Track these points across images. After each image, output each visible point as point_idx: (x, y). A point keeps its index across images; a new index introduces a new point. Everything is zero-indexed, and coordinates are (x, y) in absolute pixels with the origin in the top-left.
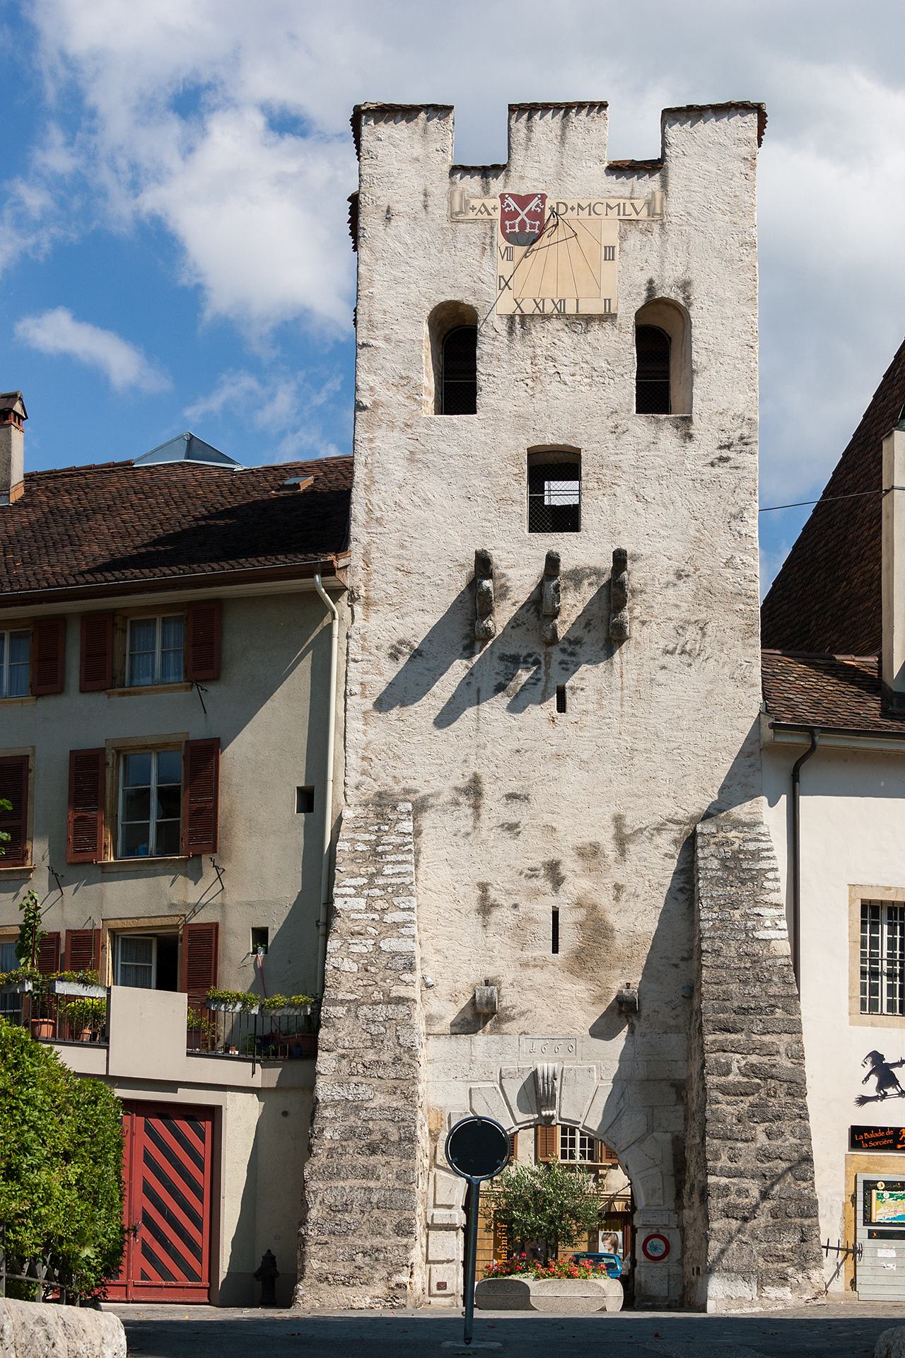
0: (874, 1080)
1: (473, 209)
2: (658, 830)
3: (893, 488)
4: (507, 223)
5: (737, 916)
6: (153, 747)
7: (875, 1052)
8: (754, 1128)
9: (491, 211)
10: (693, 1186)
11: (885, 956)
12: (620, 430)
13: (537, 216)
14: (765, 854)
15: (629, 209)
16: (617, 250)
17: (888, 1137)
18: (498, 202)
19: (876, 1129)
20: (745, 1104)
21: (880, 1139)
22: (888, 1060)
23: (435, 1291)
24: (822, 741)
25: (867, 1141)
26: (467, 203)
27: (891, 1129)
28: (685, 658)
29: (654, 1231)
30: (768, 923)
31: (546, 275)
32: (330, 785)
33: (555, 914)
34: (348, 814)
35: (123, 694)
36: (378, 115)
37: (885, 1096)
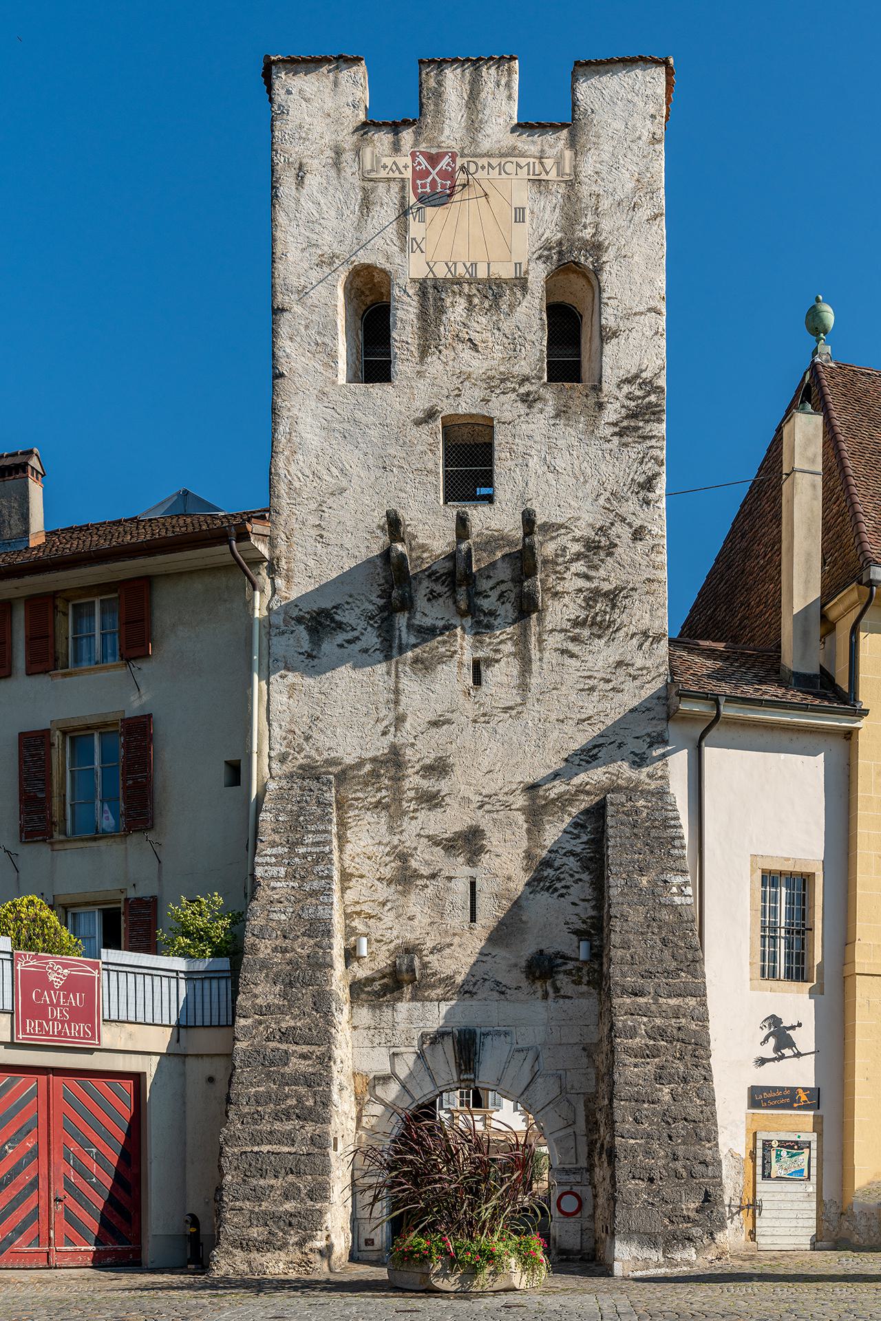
0: (772, 1041)
1: (385, 167)
3: (793, 470)
4: (419, 182)
5: (645, 882)
6: (96, 727)
7: (773, 1016)
9: (403, 170)
10: (602, 1145)
12: (531, 398)
13: (448, 175)
14: (672, 822)
15: (538, 168)
16: (527, 212)
17: (784, 1097)
18: (408, 160)
19: (774, 1089)
20: (651, 1068)
21: (776, 1098)
22: (786, 1023)
23: (363, 1247)
24: (728, 711)
25: (766, 1100)
26: (378, 161)
28: (595, 630)
29: (567, 1188)
32: (255, 756)
33: (473, 885)
34: (272, 785)
35: (65, 675)
36: (288, 66)
37: (783, 1057)
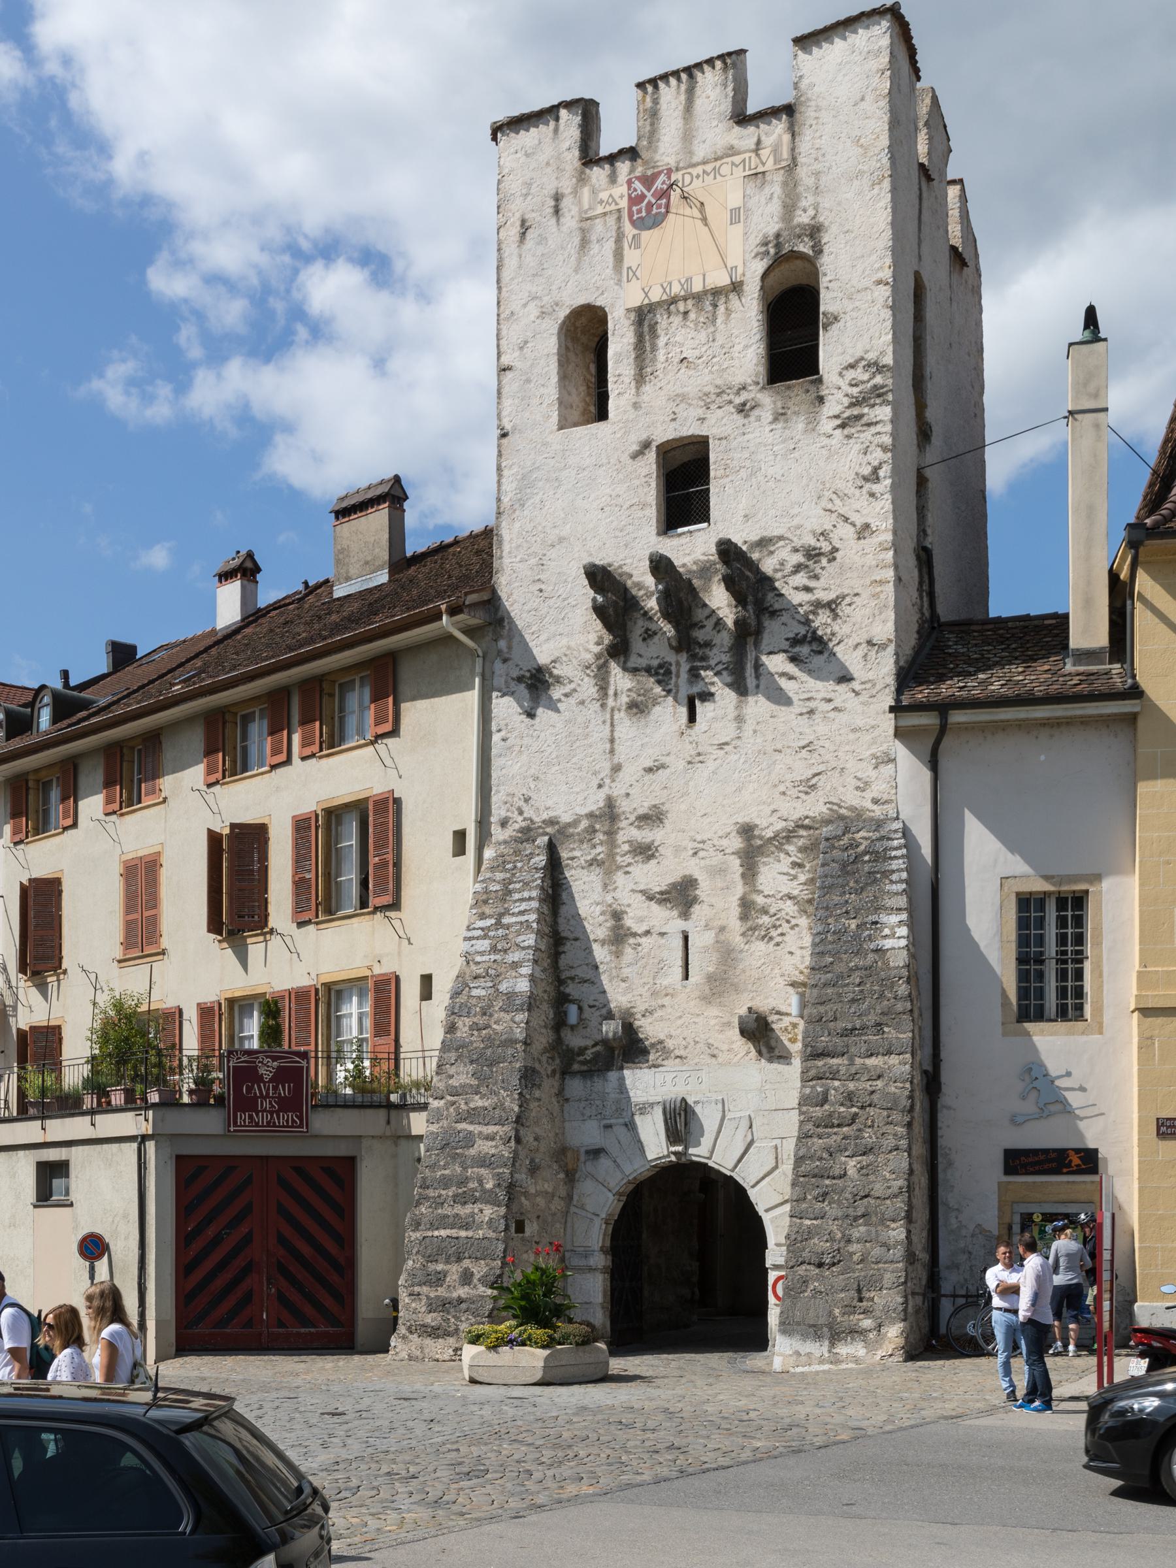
1: (601, 202)
2: (788, 838)
4: (635, 209)
8: (845, 1163)
9: (618, 200)
11: (1053, 954)
19: (1035, 1152)
27: (1055, 1150)
30: (887, 931)
31: (677, 256)
